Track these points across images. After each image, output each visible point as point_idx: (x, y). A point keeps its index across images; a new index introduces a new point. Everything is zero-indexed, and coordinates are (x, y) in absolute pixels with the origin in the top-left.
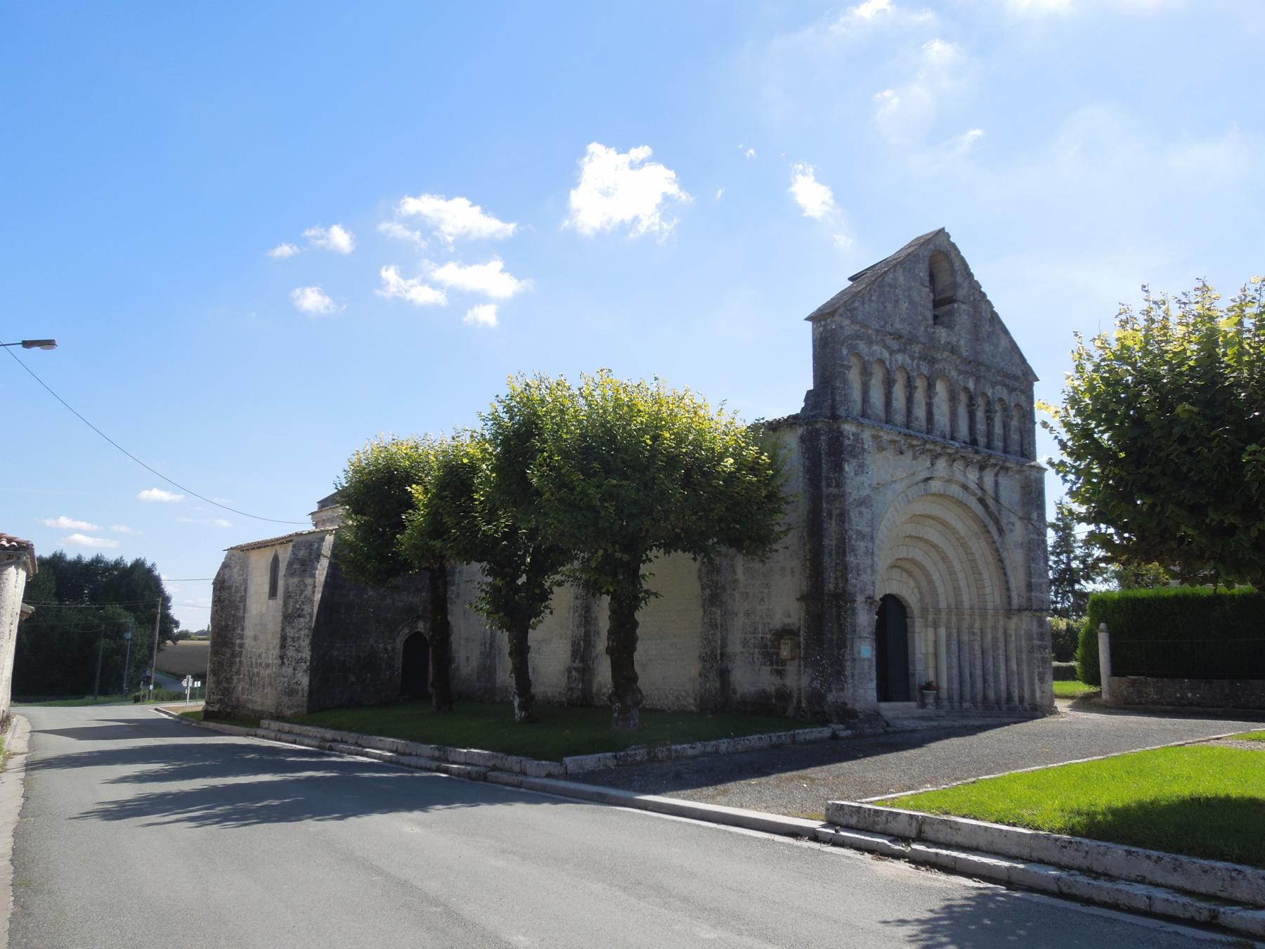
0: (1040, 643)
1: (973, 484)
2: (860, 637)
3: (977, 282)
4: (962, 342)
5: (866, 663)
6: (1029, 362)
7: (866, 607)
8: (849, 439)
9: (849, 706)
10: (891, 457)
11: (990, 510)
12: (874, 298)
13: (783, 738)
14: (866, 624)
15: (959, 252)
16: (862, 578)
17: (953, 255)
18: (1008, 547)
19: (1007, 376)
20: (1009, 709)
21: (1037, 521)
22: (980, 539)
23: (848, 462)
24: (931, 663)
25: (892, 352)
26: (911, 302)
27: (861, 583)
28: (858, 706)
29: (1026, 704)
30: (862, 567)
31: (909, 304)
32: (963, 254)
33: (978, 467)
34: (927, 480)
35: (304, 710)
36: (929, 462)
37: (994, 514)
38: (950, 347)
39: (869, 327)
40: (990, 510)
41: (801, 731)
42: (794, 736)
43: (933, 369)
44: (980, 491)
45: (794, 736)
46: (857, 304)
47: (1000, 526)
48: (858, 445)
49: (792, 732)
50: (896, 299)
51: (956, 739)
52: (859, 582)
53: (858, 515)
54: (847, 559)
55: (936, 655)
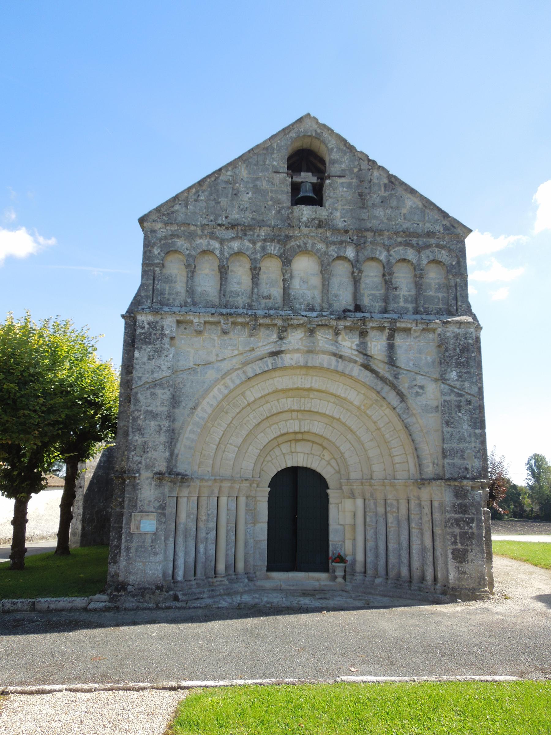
0: (461, 515)
1: (349, 351)
2: (142, 511)
3: (361, 153)
4: (338, 214)
5: (148, 536)
6: (452, 213)
7: (154, 483)
8: (143, 328)
9: (121, 579)
10: (216, 338)
11: (380, 375)
12: (202, 198)
13: (19, 605)
14: (152, 499)
15: (332, 131)
16: (149, 455)
17: (326, 135)
18: (414, 412)
19: (408, 234)
20: (420, 590)
21: (457, 380)
22: (382, 406)
23: (140, 349)
24: (348, 535)
25: (222, 242)
26: (257, 190)
27: (148, 460)
28: (131, 579)
29: (439, 586)
30: (150, 445)
31: (254, 193)
32: (336, 131)
33: (358, 333)
34: (275, 354)
35: (79, 545)
36: (275, 336)
37: (386, 379)
38: (317, 222)
39: (189, 224)
40: (380, 375)
41: (43, 600)
42: (34, 603)
43: (288, 247)
44: (361, 356)
45: (34, 603)
46: (177, 207)
47: (399, 390)
48: (155, 332)
49: (33, 600)
50: (234, 193)
51: (57, 634)
52: (145, 459)
53: (149, 397)
54: (130, 438)
55: (354, 526)
